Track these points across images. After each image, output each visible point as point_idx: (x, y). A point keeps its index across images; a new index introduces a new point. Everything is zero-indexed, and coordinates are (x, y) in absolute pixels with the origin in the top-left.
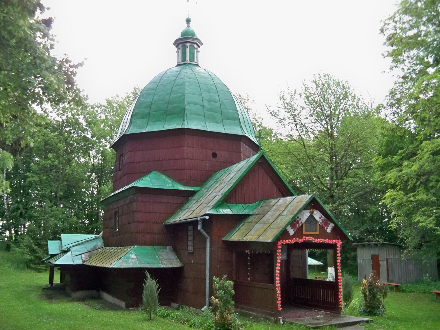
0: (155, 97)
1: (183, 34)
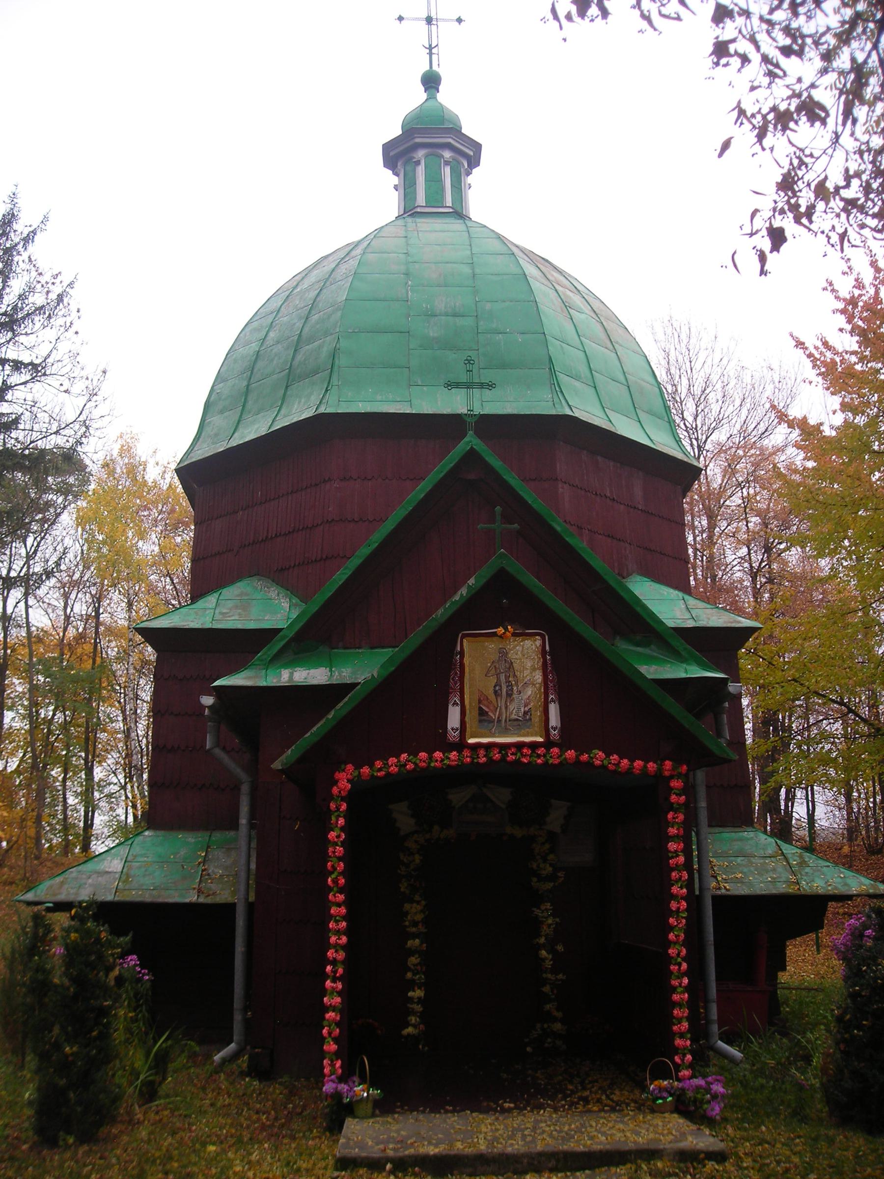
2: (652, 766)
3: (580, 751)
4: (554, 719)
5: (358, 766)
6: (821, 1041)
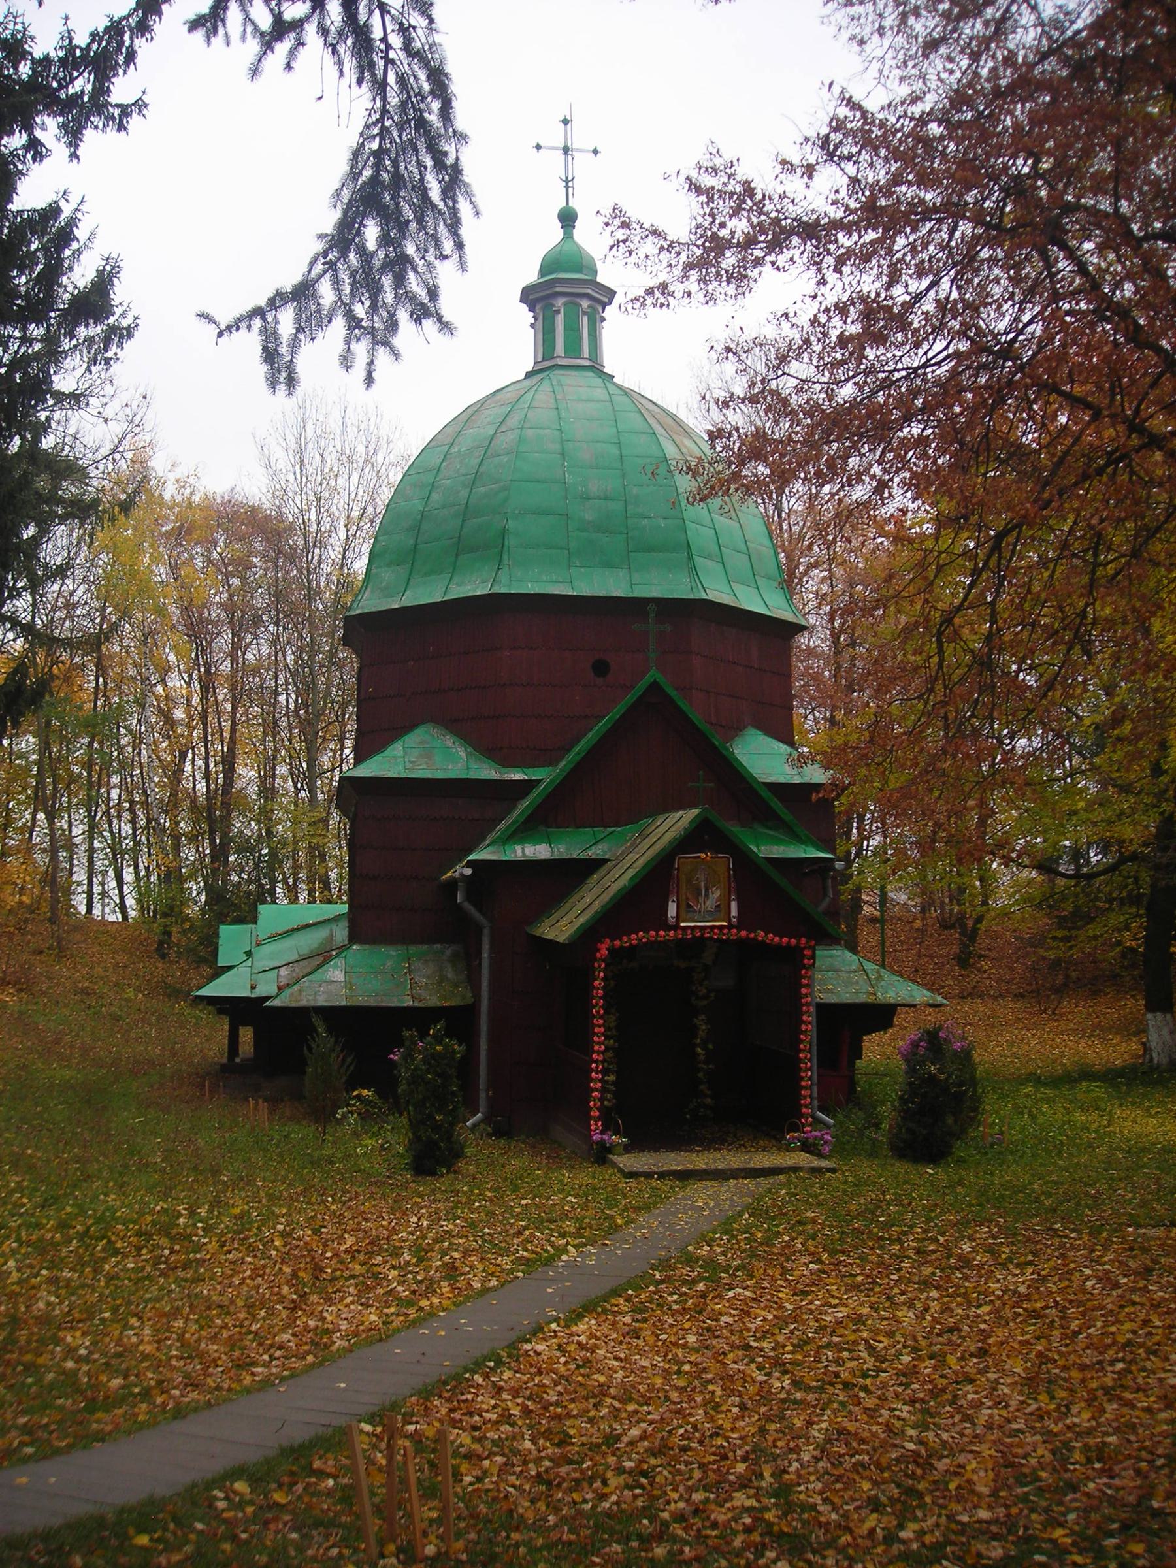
0: (435, 496)
1: (544, 269)
2: (794, 941)
3: (750, 930)
4: (734, 913)
5: (613, 940)
6: (887, 1112)
